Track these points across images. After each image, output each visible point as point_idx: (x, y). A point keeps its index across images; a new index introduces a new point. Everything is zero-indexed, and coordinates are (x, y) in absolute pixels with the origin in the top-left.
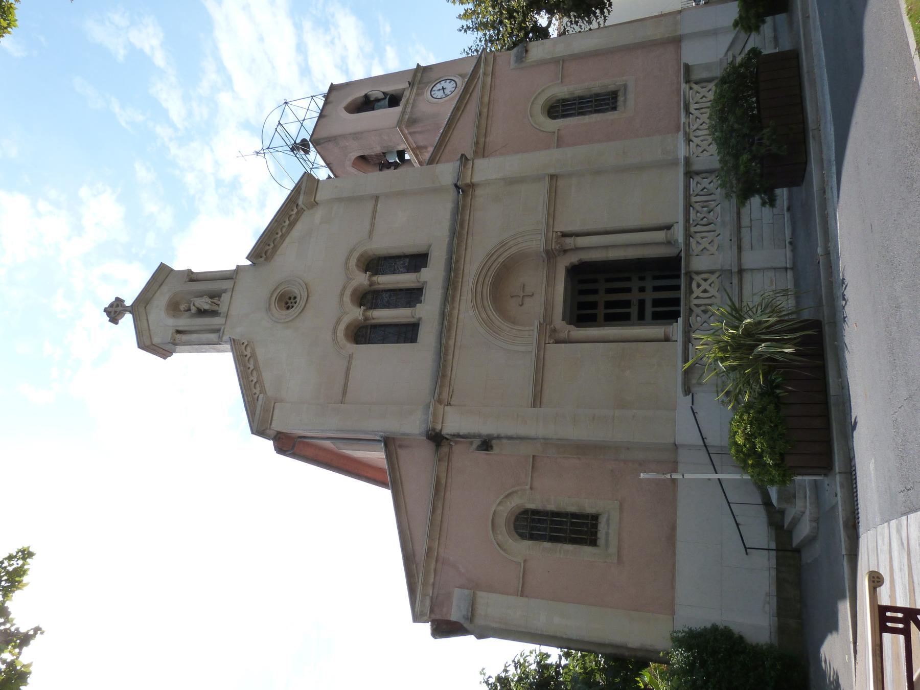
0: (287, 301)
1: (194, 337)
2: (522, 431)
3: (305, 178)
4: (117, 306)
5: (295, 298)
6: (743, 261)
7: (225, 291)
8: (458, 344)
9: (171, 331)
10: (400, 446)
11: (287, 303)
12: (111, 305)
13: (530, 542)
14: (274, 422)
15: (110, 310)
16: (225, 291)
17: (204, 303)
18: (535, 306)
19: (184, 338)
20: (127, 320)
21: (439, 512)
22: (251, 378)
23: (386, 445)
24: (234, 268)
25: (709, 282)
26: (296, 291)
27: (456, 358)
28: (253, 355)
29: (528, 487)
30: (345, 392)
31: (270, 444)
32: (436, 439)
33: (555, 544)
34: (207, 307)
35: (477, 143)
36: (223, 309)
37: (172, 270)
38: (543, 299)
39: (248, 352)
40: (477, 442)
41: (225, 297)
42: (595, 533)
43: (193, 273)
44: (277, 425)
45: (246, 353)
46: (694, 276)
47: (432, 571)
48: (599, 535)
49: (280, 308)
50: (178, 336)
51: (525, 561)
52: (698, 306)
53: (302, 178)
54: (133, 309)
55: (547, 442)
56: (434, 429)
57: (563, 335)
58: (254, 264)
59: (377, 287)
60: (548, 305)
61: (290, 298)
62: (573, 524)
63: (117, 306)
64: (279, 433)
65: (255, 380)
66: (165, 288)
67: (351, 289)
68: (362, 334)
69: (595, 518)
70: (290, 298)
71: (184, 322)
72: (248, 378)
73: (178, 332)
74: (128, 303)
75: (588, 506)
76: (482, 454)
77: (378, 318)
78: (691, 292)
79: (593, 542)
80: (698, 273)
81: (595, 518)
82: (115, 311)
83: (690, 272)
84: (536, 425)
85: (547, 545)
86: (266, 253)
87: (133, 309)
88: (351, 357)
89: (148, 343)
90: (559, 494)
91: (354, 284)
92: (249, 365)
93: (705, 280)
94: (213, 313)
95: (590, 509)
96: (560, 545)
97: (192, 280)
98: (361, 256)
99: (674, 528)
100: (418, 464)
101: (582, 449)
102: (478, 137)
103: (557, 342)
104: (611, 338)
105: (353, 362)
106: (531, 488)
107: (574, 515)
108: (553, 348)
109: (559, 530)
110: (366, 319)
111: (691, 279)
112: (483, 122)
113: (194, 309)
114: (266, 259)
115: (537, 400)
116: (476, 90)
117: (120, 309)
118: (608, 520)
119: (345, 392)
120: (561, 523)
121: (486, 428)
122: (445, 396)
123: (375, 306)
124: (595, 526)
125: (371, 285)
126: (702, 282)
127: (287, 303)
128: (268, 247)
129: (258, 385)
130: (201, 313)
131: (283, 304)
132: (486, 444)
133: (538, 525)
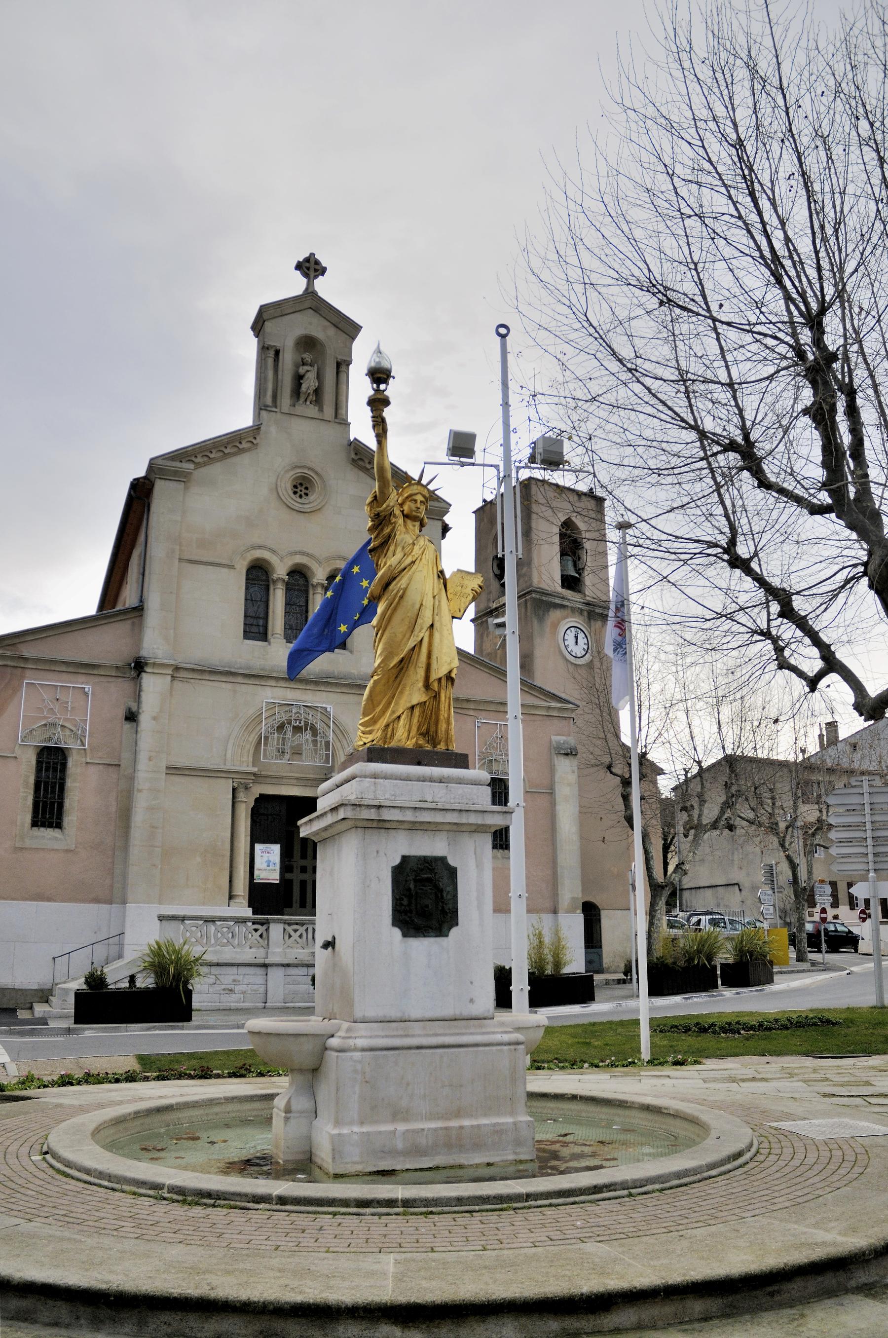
0: (302, 486)
1: (270, 374)
2: (143, 757)
3: (443, 505)
4: (316, 270)
5: (306, 494)
6: (275, 968)
7: (321, 410)
8: (238, 687)
9: (278, 345)
10: (133, 624)
11: (301, 484)
12: (317, 262)
13: (34, 762)
14: (163, 481)
15: (312, 260)
16: (321, 410)
17: (309, 383)
18: (274, 763)
19: (270, 361)
20: (296, 285)
21: (64, 668)
22: (214, 451)
23: (134, 609)
24: (349, 421)
25: (299, 940)
26: (314, 497)
27: (224, 685)
28: (241, 451)
29: (88, 760)
30: (191, 562)
31: (141, 473)
32: (139, 666)
33: (32, 787)
34: (304, 388)
35: (468, 701)
36: (300, 409)
37: (353, 339)
38: (284, 774)
39: (244, 445)
40: (134, 709)
41: (312, 411)
42: (43, 825)
43: (348, 365)
44: (160, 487)
45: (243, 442)
46: (265, 927)
47: (5, 663)
48: (42, 829)
49: (295, 479)
50: (272, 353)
51: (16, 758)
52: (307, 930)
53: (444, 501)
54: (310, 293)
55: (132, 779)
56: (146, 664)
57: (241, 796)
58: (350, 444)
59: (311, 592)
60: (278, 779)
61: (307, 488)
62: (52, 804)
63: (316, 270)
64: (152, 485)
65: (212, 456)
66: (332, 331)
67: (309, 564)
68: (258, 574)
69: (59, 826)
70: (307, 488)
71: (288, 358)
72: (214, 448)
73: (277, 353)
74: (321, 285)
75: (70, 819)
76: (121, 713)
77: (274, 595)
78: (289, 924)
79: (35, 824)
80: (267, 930)
81: (59, 826)
82: (310, 267)
83: (269, 923)
84: (147, 772)
85: (32, 780)
86: (360, 459)
87: (310, 293)
88: (231, 567)
89: (265, 316)
90: (82, 789)
91: (314, 566)
92: (229, 446)
93: (261, 936)
94: (296, 392)
95: (67, 820)
96: (32, 792)
97: (339, 365)
98: (308, 568)
99: (49, 899)
100: (109, 645)
101: (125, 815)
102: (475, 701)
103: (234, 790)
104: (236, 844)
105: (226, 570)
106: (87, 763)
107: (61, 806)
108: (224, 788)
109: (46, 790)
110: (275, 582)
111: (262, 924)
112: (492, 707)
113: (302, 370)
114: (353, 460)
115: (173, 770)
116: (535, 699)
117: (312, 274)
118: (56, 838)
119: (191, 562)
120: (53, 792)
121: (145, 719)
122: (182, 674)
123: (289, 588)
124: (50, 826)
125: (312, 585)
126: (298, 933)
127: (301, 484)
128: (367, 461)
129: (206, 459)
130: (298, 379)
131: (299, 482)
132: (131, 717)
133: (52, 764)
